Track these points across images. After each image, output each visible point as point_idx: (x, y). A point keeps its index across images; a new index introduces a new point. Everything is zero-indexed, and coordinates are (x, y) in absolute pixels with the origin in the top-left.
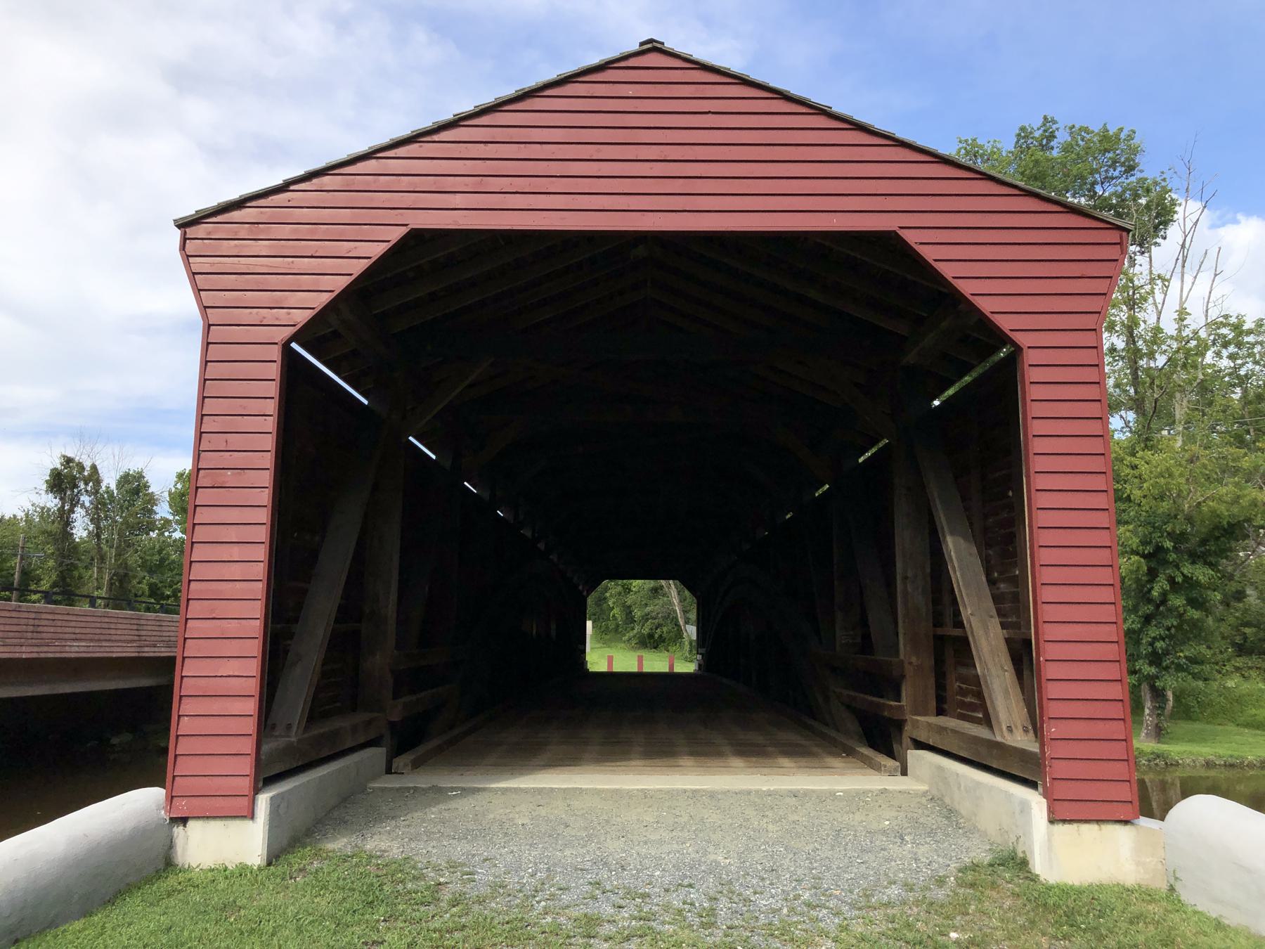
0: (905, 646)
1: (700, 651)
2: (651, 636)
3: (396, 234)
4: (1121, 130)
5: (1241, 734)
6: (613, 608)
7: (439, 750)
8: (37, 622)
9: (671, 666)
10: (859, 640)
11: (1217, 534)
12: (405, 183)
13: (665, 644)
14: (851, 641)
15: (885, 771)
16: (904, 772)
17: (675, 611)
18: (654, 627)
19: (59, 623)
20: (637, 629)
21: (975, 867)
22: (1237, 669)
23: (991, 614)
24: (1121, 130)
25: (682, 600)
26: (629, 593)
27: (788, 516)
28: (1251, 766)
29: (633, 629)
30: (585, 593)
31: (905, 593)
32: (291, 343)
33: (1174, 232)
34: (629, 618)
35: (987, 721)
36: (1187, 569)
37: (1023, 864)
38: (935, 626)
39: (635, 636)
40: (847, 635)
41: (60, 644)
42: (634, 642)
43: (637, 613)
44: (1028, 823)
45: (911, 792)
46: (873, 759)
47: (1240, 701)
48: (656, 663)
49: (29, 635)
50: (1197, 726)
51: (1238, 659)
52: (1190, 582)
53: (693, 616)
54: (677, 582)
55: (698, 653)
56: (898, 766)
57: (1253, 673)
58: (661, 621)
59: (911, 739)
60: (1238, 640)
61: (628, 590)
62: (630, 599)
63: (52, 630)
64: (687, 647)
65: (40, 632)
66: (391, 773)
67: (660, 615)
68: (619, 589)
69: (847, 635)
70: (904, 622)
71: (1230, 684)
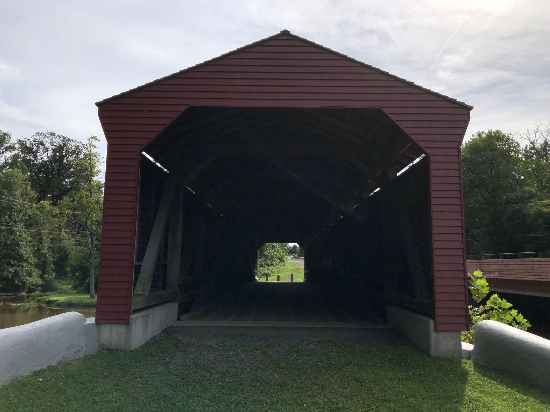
3: (182, 109)
8: (532, 266)
12: (308, 96)
19: (542, 266)
27: (342, 217)
32: (142, 152)
41: (544, 275)
49: (530, 271)
63: (539, 269)
65: (535, 270)
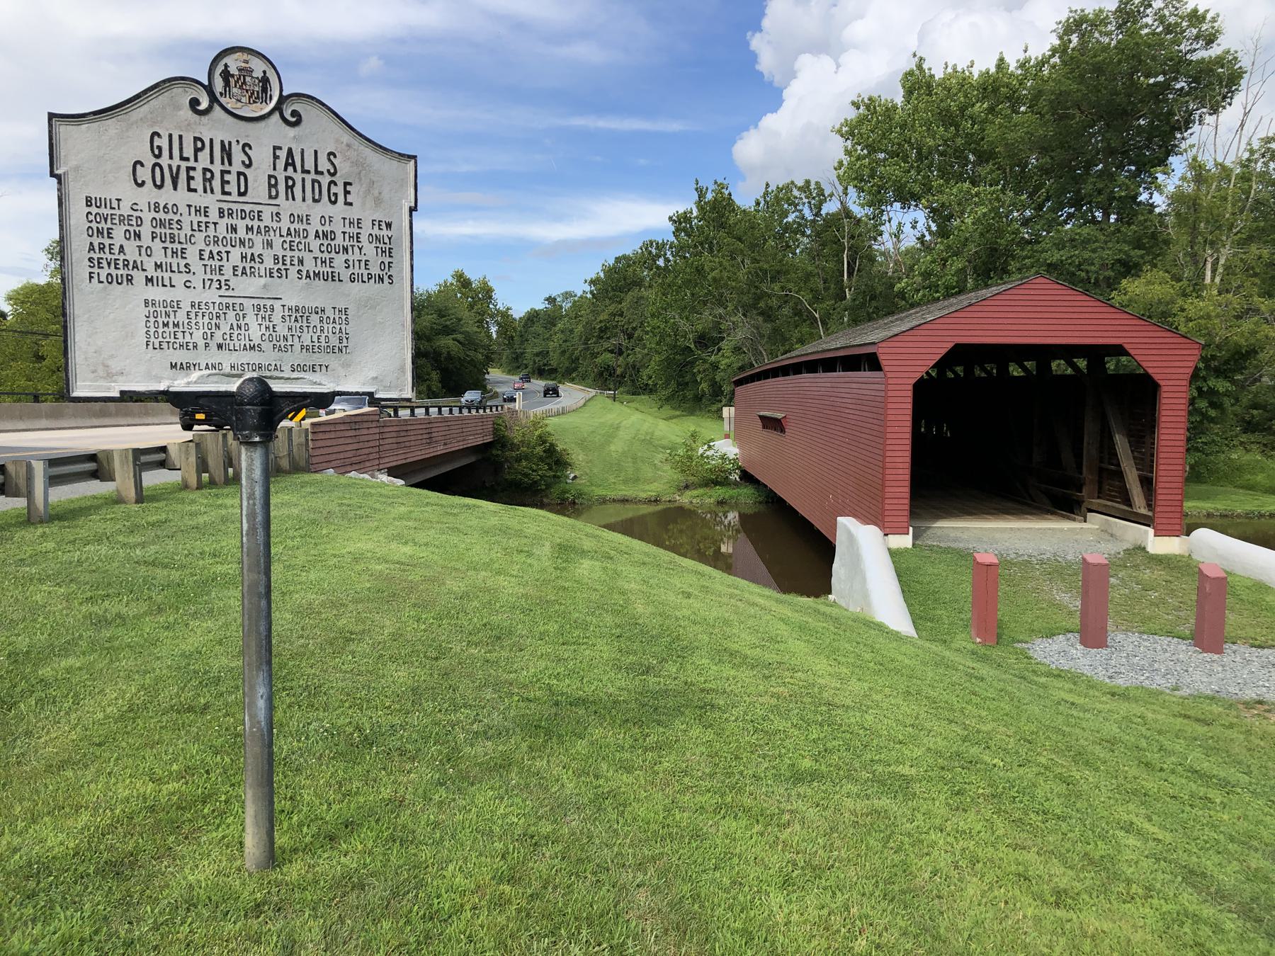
3: (950, 346)
4: (1207, 11)
5: (1235, 494)
11: (1237, 357)
21: (1128, 550)
22: (1242, 443)
24: (1207, 11)
28: (1239, 516)
33: (1239, 99)
35: (1130, 506)
36: (1212, 382)
37: (1144, 548)
44: (1147, 538)
47: (1239, 469)
50: (1204, 487)
51: (1244, 435)
52: (1212, 392)
57: (1254, 447)
60: (1247, 418)
71: (1234, 456)
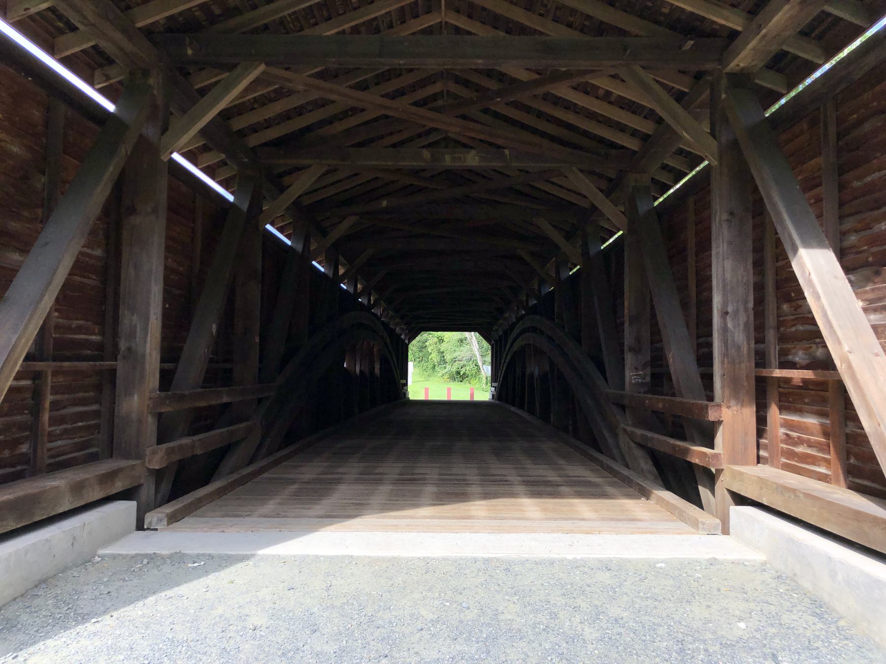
0: (723, 387)
1: (494, 384)
2: (458, 373)
6: (431, 353)
7: (221, 493)
9: (472, 395)
10: (648, 379)
13: (469, 379)
14: (640, 381)
15: (704, 529)
16: (726, 531)
17: (475, 356)
18: (460, 367)
20: (448, 367)
23: (876, 351)
25: (481, 347)
26: (443, 342)
29: (445, 368)
30: (407, 341)
31: (725, 329)
34: (443, 361)
38: (758, 365)
39: (447, 373)
40: (636, 375)
42: (446, 377)
43: (448, 357)
45: (747, 563)
46: (685, 512)
48: (460, 393)
53: (489, 359)
54: (477, 334)
55: (492, 386)
56: (718, 524)
58: (465, 362)
59: (727, 489)
61: (441, 340)
62: (443, 347)
64: (484, 381)
66: (143, 529)
67: (464, 359)
68: (436, 340)
69: (636, 375)
70: (723, 363)
